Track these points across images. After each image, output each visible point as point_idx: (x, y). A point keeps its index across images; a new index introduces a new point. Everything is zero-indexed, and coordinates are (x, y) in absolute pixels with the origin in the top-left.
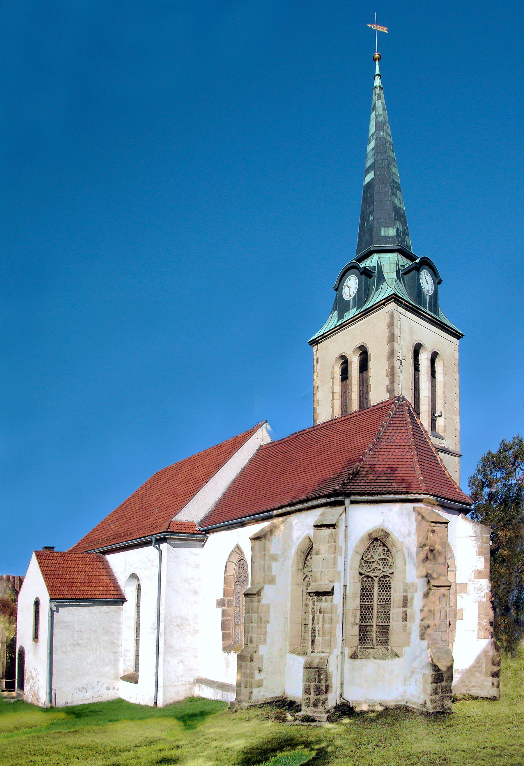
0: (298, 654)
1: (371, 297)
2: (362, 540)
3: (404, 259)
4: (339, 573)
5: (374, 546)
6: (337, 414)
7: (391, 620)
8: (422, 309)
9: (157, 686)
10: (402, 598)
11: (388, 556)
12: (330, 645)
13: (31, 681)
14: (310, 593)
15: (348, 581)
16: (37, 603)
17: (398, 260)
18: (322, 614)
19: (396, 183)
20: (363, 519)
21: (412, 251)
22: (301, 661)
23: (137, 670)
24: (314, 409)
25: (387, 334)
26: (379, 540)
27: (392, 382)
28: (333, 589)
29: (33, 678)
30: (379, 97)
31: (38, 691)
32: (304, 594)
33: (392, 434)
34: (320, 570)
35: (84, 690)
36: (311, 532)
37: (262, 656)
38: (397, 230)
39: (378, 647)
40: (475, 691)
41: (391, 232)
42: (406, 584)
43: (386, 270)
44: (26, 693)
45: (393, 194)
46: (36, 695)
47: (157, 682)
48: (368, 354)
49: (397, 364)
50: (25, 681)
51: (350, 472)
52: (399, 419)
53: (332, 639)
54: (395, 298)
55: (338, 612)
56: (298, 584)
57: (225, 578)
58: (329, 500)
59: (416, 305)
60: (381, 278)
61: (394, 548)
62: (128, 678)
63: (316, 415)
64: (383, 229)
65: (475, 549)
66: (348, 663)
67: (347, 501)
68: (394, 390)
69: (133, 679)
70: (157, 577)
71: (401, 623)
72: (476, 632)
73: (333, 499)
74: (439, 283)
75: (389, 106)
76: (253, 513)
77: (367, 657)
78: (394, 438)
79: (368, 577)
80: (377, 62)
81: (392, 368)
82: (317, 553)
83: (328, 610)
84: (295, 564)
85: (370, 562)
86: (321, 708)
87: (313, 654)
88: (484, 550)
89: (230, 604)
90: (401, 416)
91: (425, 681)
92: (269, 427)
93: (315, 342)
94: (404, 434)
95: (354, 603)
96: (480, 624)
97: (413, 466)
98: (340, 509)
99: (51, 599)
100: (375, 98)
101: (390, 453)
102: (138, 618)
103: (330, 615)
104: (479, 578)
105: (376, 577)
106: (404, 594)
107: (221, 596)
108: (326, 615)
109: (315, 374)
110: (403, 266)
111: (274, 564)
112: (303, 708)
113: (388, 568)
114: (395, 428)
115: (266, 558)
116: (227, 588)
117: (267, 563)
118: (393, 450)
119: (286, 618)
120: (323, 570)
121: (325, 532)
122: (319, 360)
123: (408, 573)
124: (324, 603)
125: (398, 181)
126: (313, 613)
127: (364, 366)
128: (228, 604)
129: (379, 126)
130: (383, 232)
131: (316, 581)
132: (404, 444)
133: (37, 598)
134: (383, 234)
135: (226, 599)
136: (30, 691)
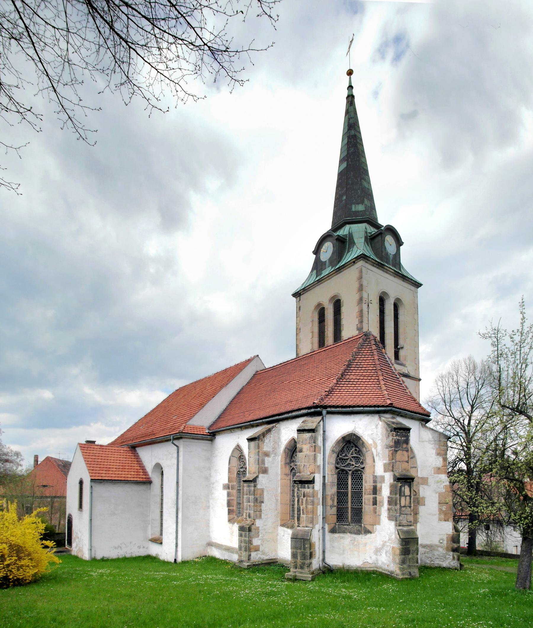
0: (288, 527)
2: (338, 442)
4: (319, 467)
5: (347, 447)
7: (363, 504)
8: (387, 265)
9: (177, 546)
10: (372, 487)
12: (312, 521)
13: (77, 540)
14: (295, 481)
15: (326, 472)
16: (81, 483)
17: (366, 228)
18: (305, 498)
20: (338, 427)
22: (290, 532)
23: (161, 534)
26: (351, 443)
27: (361, 322)
28: (314, 478)
29: (78, 538)
31: (82, 547)
32: (292, 482)
33: (360, 361)
34: (303, 464)
35: (119, 548)
36: (295, 435)
37: (258, 527)
39: (353, 524)
42: (375, 477)
46: (80, 550)
47: (177, 544)
49: (365, 307)
50: (73, 540)
51: (326, 390)
53: (314, 517)
54: (363, 257)
55: (319, 497)
56: (286, 474)
57: (229, 469)
58: (309, 411)
62: (155, 540)
64: (353, 206)
65: (434, 452)
66: (328, 536)
67: (324, 412)
68: (362, 328)
69: (158, 541)
70: (176, 466)
71: (372, 507)
72: (438, 516)
73: (312, 410)
76: (249, 420)
77: (344, 532)
78: (362, 364)
79: (343, 470)
81: (361, 311)
82: (301, 451)
83: (310, 495)
84: (284, 459)
85: (345, 459)
86: (306, 570)
87: (298, 528)
89: (233, 488)
90: (368, 347)
91: (394, 554)
95: (332, 490)
96: (440, 510)
97: (379, 385)
98: (319, 418)
99: (92, 480)
103: (312, 498)
104: (438, 474)
105: (350, 471)
106: (374, 484)
107: (226, 482)
108: (308, 498)
111: (266, 459)
112: (292, 570)
113: (359, 464)
114: (363, 356)
115: (260, 454)
116: (231, 476)
117: (260, 459)
119: (277, 500)
120: (306, 464)
121: (308, 435)
122: (301, 308)
123: (378, 466)
124: (307, 490)
128: (232, 487)
131: (300, 472)
132: (370, 368)
133: (81, 479)
134: (353, 209)
135: (230, 484)
136: (76, 547)
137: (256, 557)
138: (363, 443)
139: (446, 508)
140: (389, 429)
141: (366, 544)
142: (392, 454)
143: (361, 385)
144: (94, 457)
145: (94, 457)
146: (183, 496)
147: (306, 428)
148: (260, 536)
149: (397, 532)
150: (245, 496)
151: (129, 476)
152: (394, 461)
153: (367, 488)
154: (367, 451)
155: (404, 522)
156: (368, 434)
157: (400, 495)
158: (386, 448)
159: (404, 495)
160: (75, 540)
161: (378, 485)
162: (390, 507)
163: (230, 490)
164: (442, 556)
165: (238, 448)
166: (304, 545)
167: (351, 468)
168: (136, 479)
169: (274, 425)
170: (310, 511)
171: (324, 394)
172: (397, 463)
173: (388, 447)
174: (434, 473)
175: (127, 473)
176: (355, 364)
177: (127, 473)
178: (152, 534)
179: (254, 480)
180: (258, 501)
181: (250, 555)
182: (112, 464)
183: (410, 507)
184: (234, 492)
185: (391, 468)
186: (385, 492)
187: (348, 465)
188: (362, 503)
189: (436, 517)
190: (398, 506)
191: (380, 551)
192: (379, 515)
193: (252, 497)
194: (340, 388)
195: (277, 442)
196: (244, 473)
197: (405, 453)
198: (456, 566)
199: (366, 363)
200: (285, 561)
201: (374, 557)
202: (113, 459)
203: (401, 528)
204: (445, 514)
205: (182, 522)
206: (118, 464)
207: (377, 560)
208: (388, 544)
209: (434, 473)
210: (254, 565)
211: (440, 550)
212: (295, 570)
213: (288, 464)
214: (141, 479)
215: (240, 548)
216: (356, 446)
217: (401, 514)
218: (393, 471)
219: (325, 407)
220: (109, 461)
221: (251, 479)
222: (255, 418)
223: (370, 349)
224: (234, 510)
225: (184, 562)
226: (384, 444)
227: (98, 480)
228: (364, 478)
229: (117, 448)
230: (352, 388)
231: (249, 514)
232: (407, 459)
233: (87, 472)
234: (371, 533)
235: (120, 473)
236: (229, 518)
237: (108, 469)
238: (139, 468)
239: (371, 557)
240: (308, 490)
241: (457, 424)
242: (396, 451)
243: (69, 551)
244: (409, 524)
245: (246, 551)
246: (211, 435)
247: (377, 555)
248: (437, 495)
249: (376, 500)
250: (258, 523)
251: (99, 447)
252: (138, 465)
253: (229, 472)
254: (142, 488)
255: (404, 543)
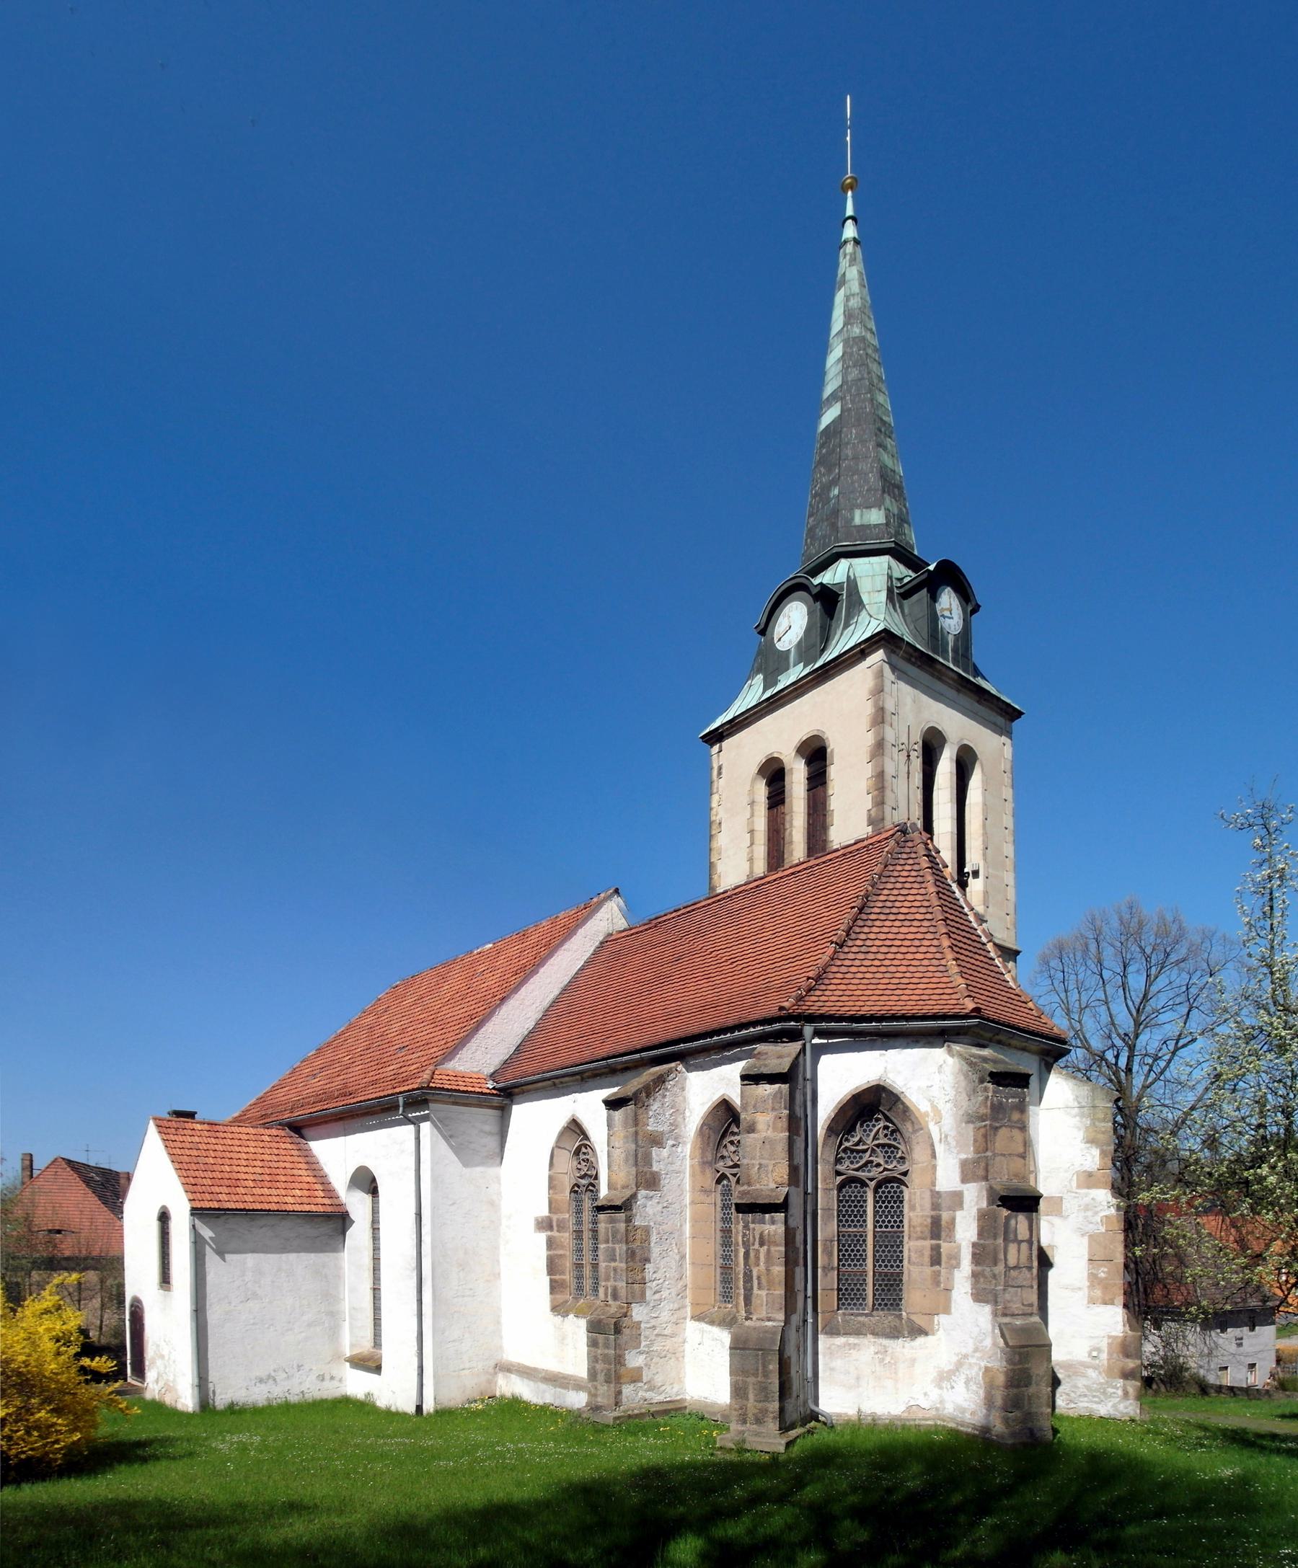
0: (712, 1323)
1: (834, 642)
3: (902, 567)
6: (760, 868)
7: (905, 1262)
10: (929, 1220)
11: (895, 1139)
13: (159, 1362)
16: (164, 1217)
17: (890, 568)
19: (884, 423)
21: (916, 553)
23: (377, 1342)
24: (711, 866)
25: (868, 709)
27: (880, 802)
29: (162, 1357)
30: (853, 261)
31: (174, 1381)
32: (719, 1209)
33: (892, 898)
35: (271, 1381)
38: (887, 510)
40: (1086, 1405)
41: (875, 517)
42: (936, 1195)
43: (865, 588)
44: (151, 1386)
45: (880, 445)
48: (829, 750)
51: (811, 974)
52: (907, 868)
54: (885, 639)
57: (551, 1179)
58: (768, 1028)
59: (917, 659)
60: (856, 604)
61: (909, 1125)
63: (715, 877)
64: (857, 513)
67: (808, 1030)
68: (883, 819)
69: (370, 1364)
71: (928, 1270)
72: (1086, 1290)
73: (777, 1026)
74: (974, 611)
75: (872, 278)
76: (605, 1055)
77: (858, 1332)
78: (897, 904)
80: (850, 193)
81: (880, 776)
82: (751, 1129)
84: (698, 1153)
85: (858, 1151)
87: (748, 1323)
88: (1101, 1136)
89: (561, 1227)
90: (911, 862)
92: (622, 903)
93: (717, 737)
94: (919, 898)
96: (1093, 1277)
99: (195, 1212)
100: (844, 263)
101: (890, 936)
102: (376, 1249)
104: (1089, 1188)
105: (871, 1180)
106: (933, 1213)
107: (544, 1211)
108: (773, 1249)
109: (715, 798)
110: (900, 580)
113: (895, 1163)
114: (899, 885)
115: (640, 1137)
116: (556, 1197)
118: (896, 930)
120: (764, 1162)
122: (724, 771)
125: (890, 419)
126: (746, 1245)
127: (818, 779)
129: (849, 317)
130: (858, 518)
131: (749, 1184)
134: (857, 521)
135: (555, 1217)
136: (157, 1381)
137: (634, 1397)
138: (906, 1110)
139: (1108, 1273)
140: (975, 1077)
141: (913, 1361)
142: (985, 1136)
143: (895, 962)
144: (195, 1153)
145: (195, 1153)
146: (433, 1248)
147: (765, 1071)
148: (643, 1344)
149: (997, 1331)
150: (602, 1246)
151: (290, 1200)
152: (989, 1154)
153: (916, 1222)
154: (915, 1131)
155: (1016, 1307)
156: (919, 1088)
157: (1005, 1239)
158: (968, 1122)
159: (1016, 1240)
160: (153, 1363)
161: (945, 1216)
162: (979, 1268)
163: (555, 1233)
164: (1097, 1390)
165: (575, 1128)
166: (764, 1366)
167: (874, 1172)
168: (307, 1208)
169: (673, 1065)
170: (777, 1280)
171: (804, 984)
172: (998, 1159)
173: (971, 1118)
174: (1079, 1187)
175: (283, 1192)
176: (880, 904)
177: (283, 1192)
178: (352, 1346)
179: (625, 1207)
180: (637, 1258)
181: (620, 1393)
182: (244, 1169)
183: (1030, 1268)
184: (566, 1237)
185: (981, 1172)
186: (966, 1231)
187: (865, 1165)
188: (901, 1261)
189: (1083, 1295)
190: (1000, 1268)
191: (949, 1379)
192: (948, 1290)
193: (620, 1249)
194: (843, 969)
195: (679, 1111)
196: (592, 1187)
197: (1016, 1132)
198: (1132, 1414)
199: (906, 904)
200: (706, 1405)
201: (935, 1394)
202: (245, 1156)
203: (1007, 1320)
204: (1106, 1287)
205: (434, 1315)
206: (259, 1170)
207: (942, 1402)
208: (972, 1360)
209: (1079, 1187)
210: (630, 1416)
211: (1092, 1373)
212: (740, 1428)
213: (710, 1164)
214: (321, 1209)
215: (593, 1374)
216: (887, 1119)
217: (1007, 1286)
218: (986, 1178)
219: (811, 1019)
220: (236, 1162)
221: (618, 1203)
222: (622, 1049)
223: (916, 867)
224: (571, 1282)
225: (443, 1413)
226: (961, 1112)
227: (210, 1209)
228: (906, 1198)
229: (252, 1131)
230: (874, 969)
231: (615, 1289)
232: (1021, 1150)
233: (180, 1189)
234: (926, 1334)
235: (266, 1191)
236: (552, 1301)
237: (235, 1183)
238: (314, 1180)
239: (925, 1394)
240: (773, 1227)
241: (1099, 1066)
242: (997, 1129)
243: (138, 1391)
244: (1028, 1310)
245: (608, 1381)
246: (507, 1093)
247: (941, 1388)
248: (1085, 1240)
249: (939, 1254)
250: (638, 1313)
251: (206, 1127)
252: (309, 1173)
253: (551, 1186)
254: (326, 1228)
255: (1017, 1357)
